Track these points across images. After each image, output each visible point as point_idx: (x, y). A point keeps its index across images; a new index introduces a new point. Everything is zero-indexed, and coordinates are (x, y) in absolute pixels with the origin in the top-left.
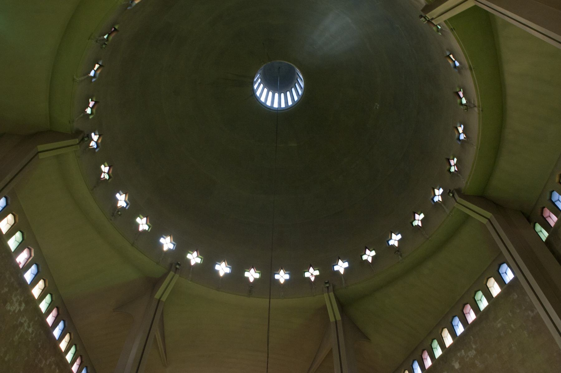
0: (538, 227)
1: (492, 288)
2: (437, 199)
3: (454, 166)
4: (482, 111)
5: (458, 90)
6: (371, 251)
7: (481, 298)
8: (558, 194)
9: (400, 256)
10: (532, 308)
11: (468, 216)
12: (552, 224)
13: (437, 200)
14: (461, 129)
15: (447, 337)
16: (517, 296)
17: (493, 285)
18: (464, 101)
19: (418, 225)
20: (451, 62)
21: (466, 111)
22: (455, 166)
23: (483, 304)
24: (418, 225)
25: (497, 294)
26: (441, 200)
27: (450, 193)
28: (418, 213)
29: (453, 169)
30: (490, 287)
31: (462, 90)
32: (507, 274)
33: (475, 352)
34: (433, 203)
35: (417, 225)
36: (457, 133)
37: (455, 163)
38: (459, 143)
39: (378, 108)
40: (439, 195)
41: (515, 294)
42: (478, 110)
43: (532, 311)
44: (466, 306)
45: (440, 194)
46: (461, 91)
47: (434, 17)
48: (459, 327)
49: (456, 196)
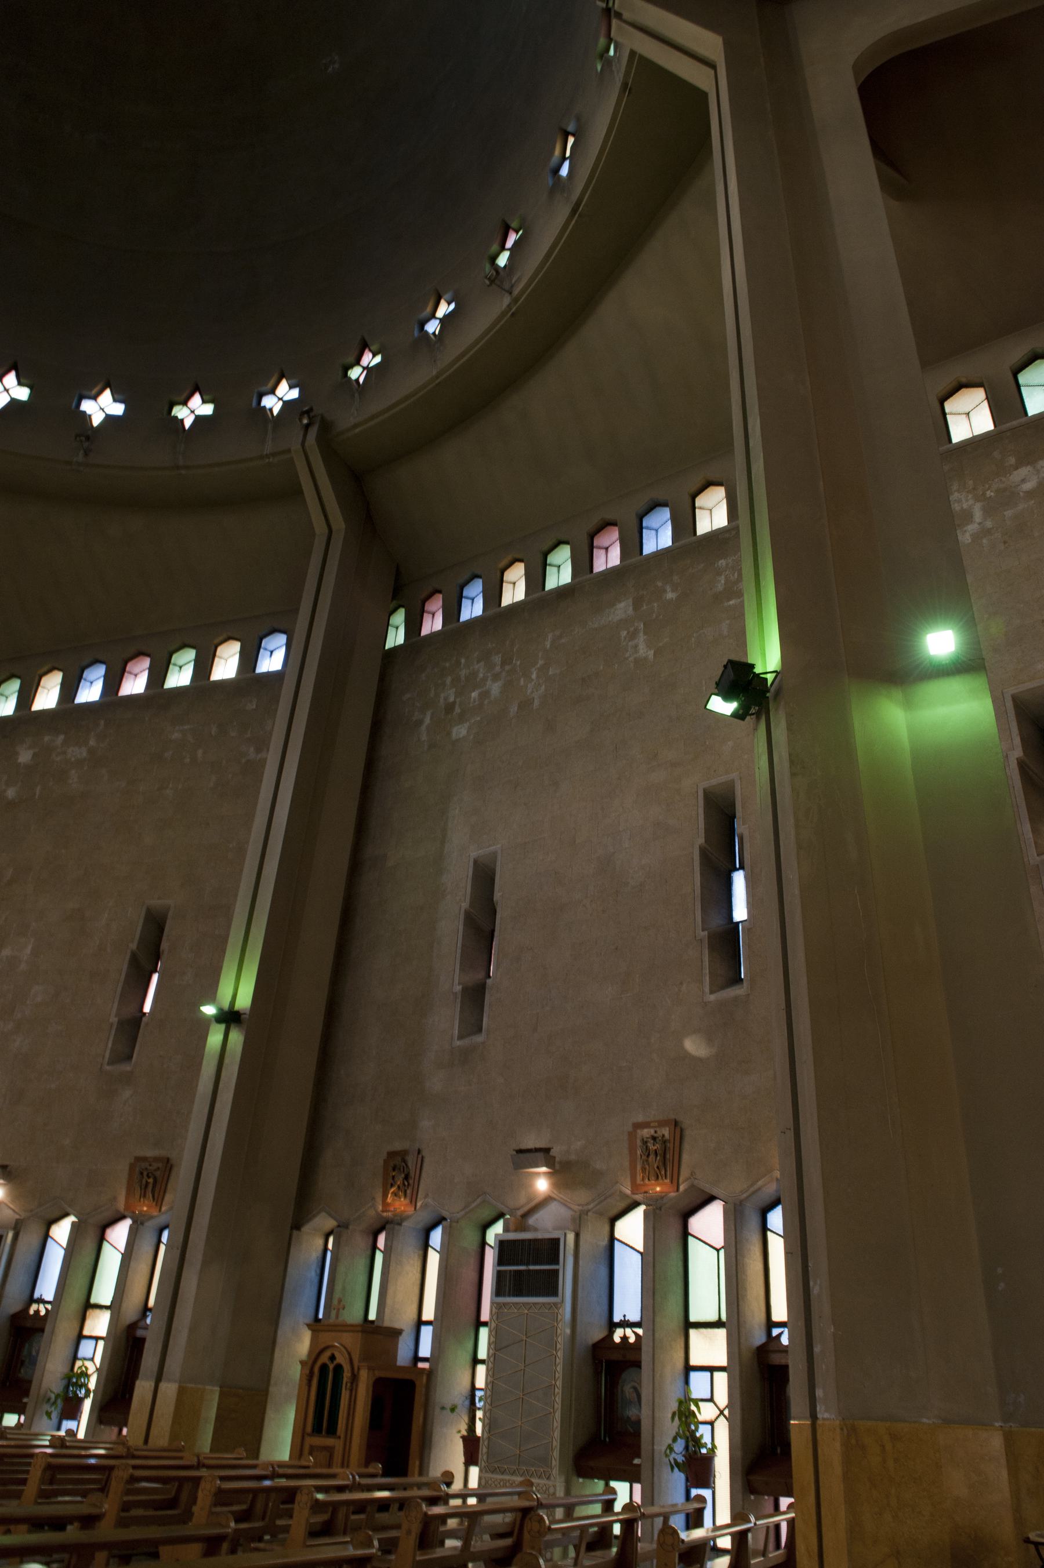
0: (399, 618)
1: (223, 661)
2: (272, 403)
3: (364, 368)
4: (513, 314)
5: (514, 225)
6: (20, 384)
7: (186, 664)
8: (481, 588)
9: (82, 452)
10: (262, 744)
11: (297, 492)
12: (425, 631)
13: (268, 406)
14: (444, 309)
15: (49, 690)
16: (254, 707)
17: (228, 658)
18: (502, 260)
19: (182, 421)
20: (557, 152)
21: (487, 282)
22: (365, 372)
23: (180, 677)
24: (182, 421)
25: (221, 679)
26: (276, 412)
27: (306, 415)
28: (204, 397)
29: (355, 373)
30: (220, 658)
31: (521, 232)
32: (273, 657)
33: (85, 754)
34: (254, 404)
35: (180, 417)
36: (429, 309)
37: (371, 365)
38: (416, 333)
39: (330, 69)
40: (280, 399)
41: (254, 703)
42: (509, 306)
43: (258, 750)
44: (141, 657)
45: (286, 398)
46: (517, 232)
47: (626, 15)
48: (92, 688)
49: (313, 432)
